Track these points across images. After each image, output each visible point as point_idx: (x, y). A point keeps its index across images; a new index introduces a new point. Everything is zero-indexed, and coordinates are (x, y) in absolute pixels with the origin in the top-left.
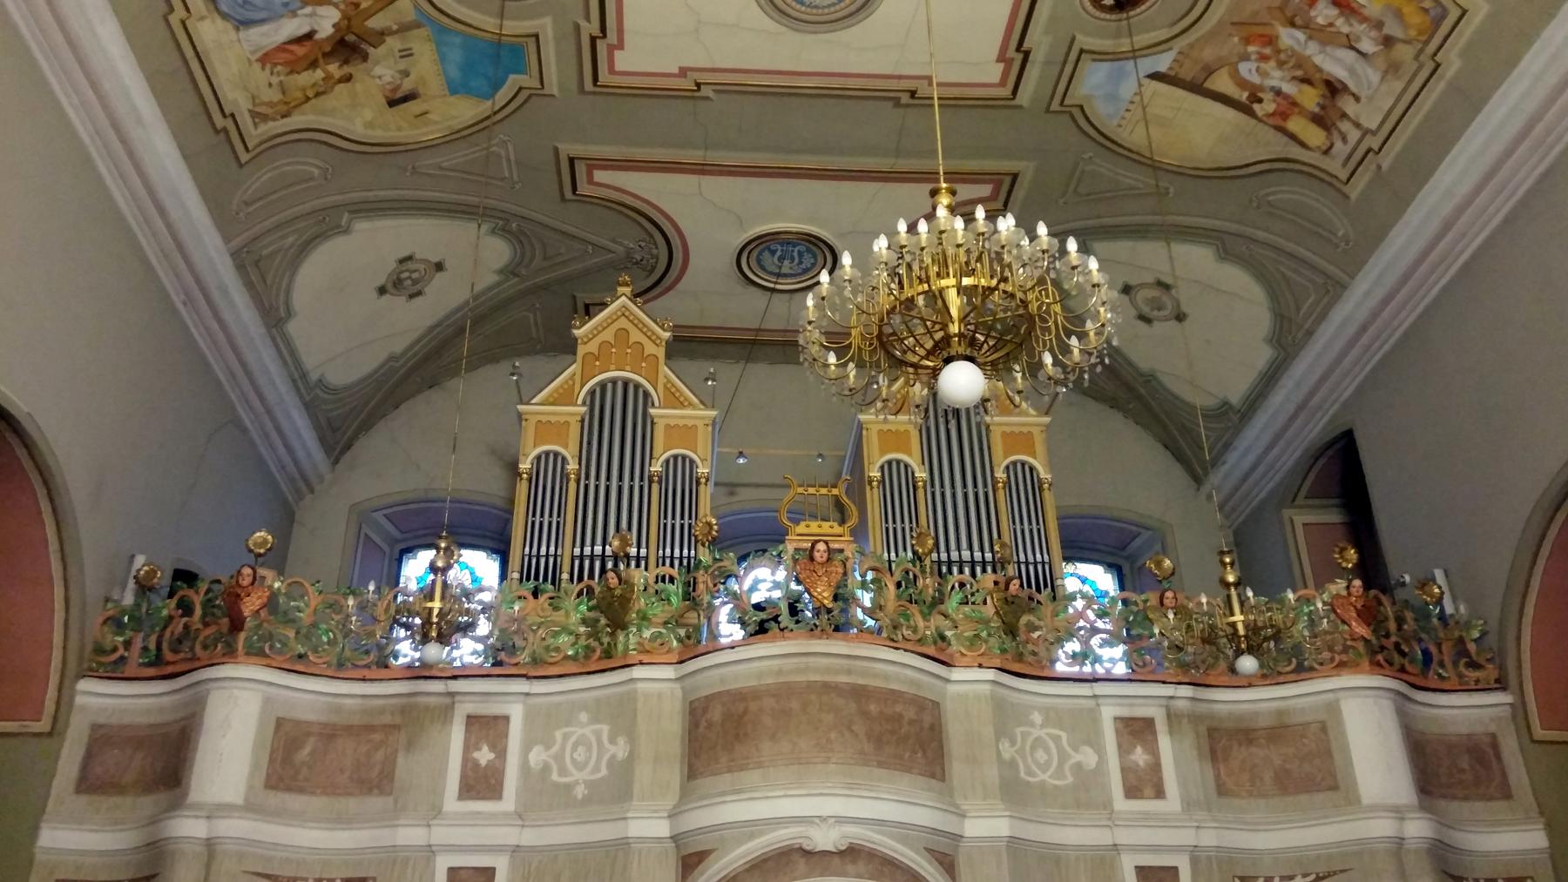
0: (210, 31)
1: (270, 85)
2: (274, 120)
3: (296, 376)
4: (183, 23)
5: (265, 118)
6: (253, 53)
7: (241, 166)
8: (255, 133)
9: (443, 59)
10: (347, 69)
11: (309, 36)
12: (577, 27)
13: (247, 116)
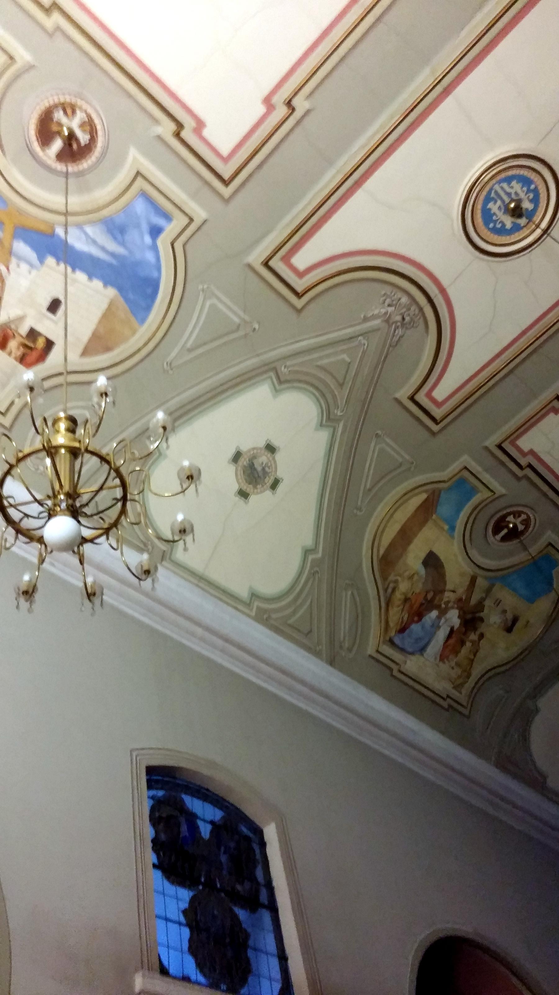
0: (412, 665)
1: (453, 668)
2: (466, 682)
3: (196, 582)
4: (400, 671)
5: (462, 685)
6: (436, 658)
7: (468, 717)
8: (462, 696)
9: (514, 590)
10: (478, 633)
11: (452, 631)
12: (159, 138)
13: (454, 691)
